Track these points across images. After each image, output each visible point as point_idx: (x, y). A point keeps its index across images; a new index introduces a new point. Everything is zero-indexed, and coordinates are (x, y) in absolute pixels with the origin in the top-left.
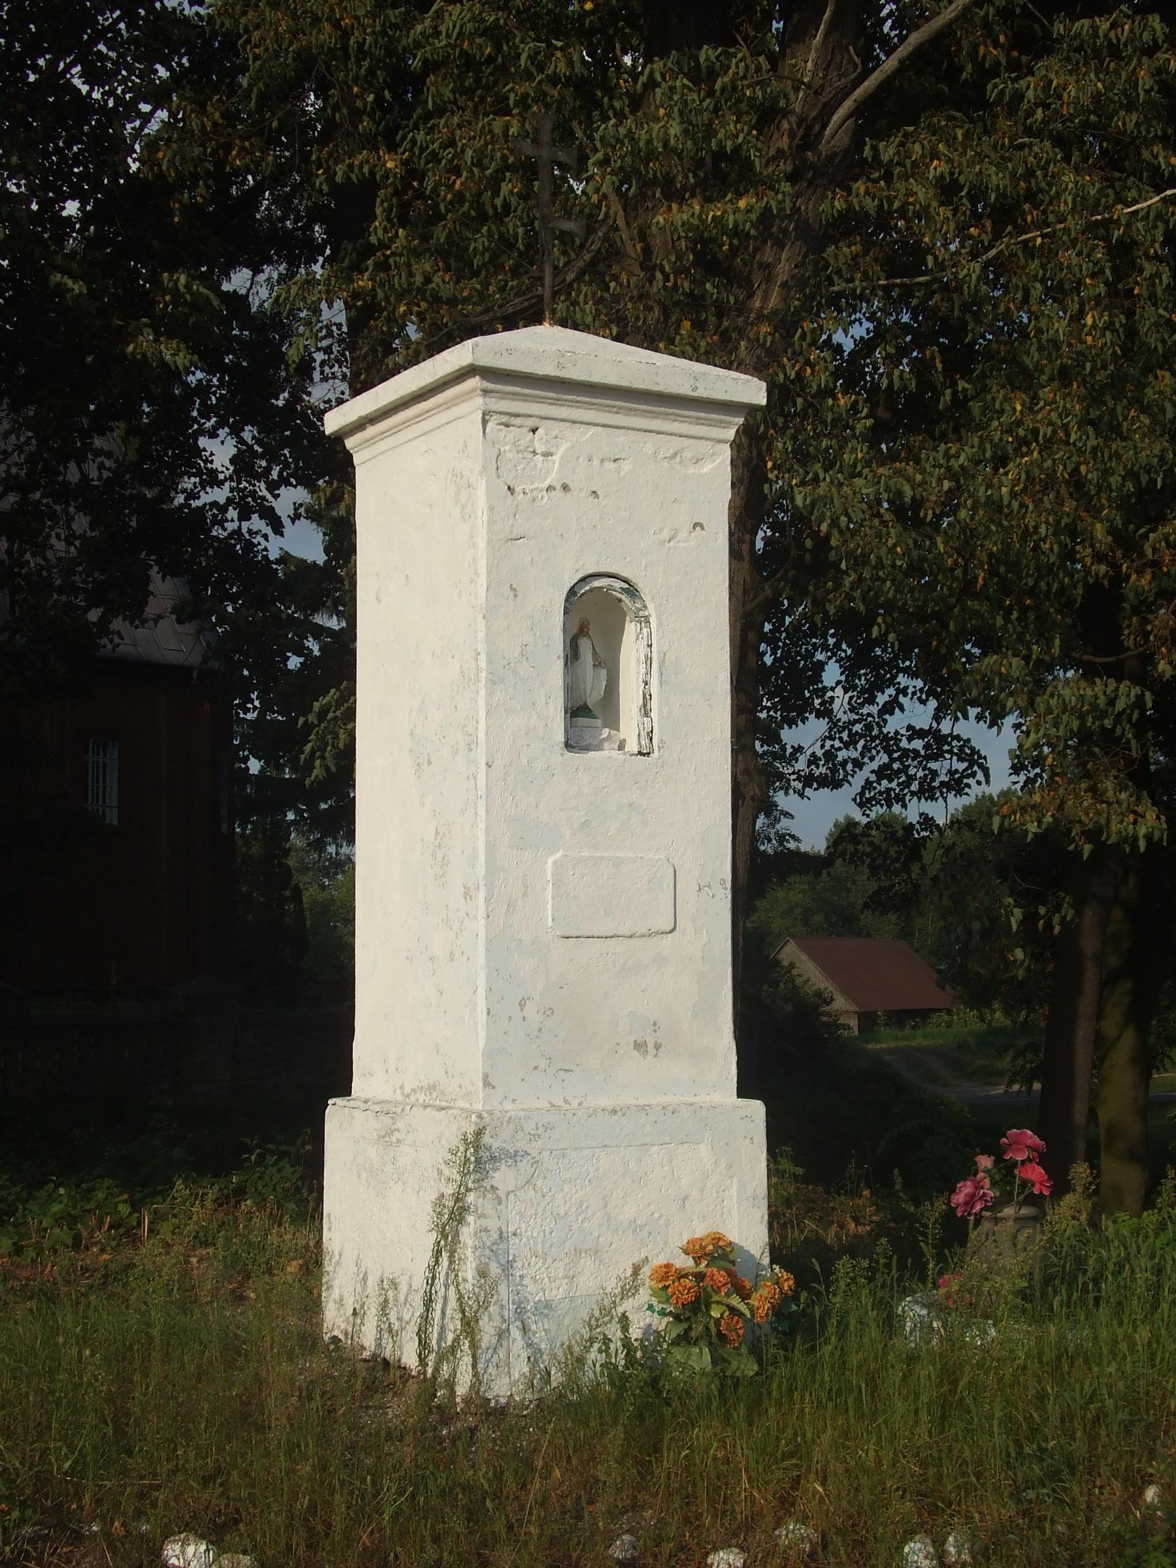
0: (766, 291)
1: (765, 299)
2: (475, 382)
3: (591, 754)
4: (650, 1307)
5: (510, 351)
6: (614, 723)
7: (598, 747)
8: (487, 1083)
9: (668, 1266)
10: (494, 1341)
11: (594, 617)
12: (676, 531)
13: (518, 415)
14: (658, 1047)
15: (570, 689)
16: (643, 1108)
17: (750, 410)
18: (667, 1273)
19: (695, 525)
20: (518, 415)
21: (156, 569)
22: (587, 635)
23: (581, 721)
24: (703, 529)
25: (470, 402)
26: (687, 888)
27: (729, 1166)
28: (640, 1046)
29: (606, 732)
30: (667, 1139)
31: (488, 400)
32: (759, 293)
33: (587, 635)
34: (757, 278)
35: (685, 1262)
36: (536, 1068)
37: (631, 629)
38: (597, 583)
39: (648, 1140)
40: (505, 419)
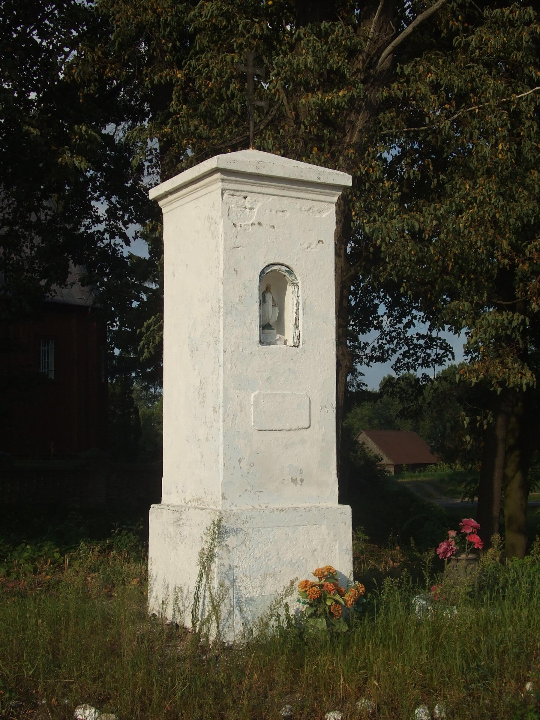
0: (352, 134)
1: (351, 137)
2: (218, 175)
3: (271, 346)
4: (299, 600)
5: (234, 161)
6: (282, 332)
7: (275, 343)
8: (224, 498)
9: (307, 581)
10: (227, 616)
11: (273, 283)
12: (311, 244)
13: (238, 191)
14: (302, 481)
15: (262, 316)
16: (295, 509)
17: (344, 188)
18: (306, 585)
19: (319, 241)
20: (238, 191)
21: (72, 261)
22: (270, 292)
23: (267, 331)
24: (323, 243)
25: (216, 185)
26: (315, 408)
27: (335, 536)
28: (294, 480)
29: (278, 336)
30: (306, 523)
31: (224, 184)
32: (349, 135)
33: (270, 292)
34: (348, 128)
35: (315, 580)
36: (246, 490)
37: (290, 289)
38: (274, 268)
39: (298, 523)
40: (232, 192)
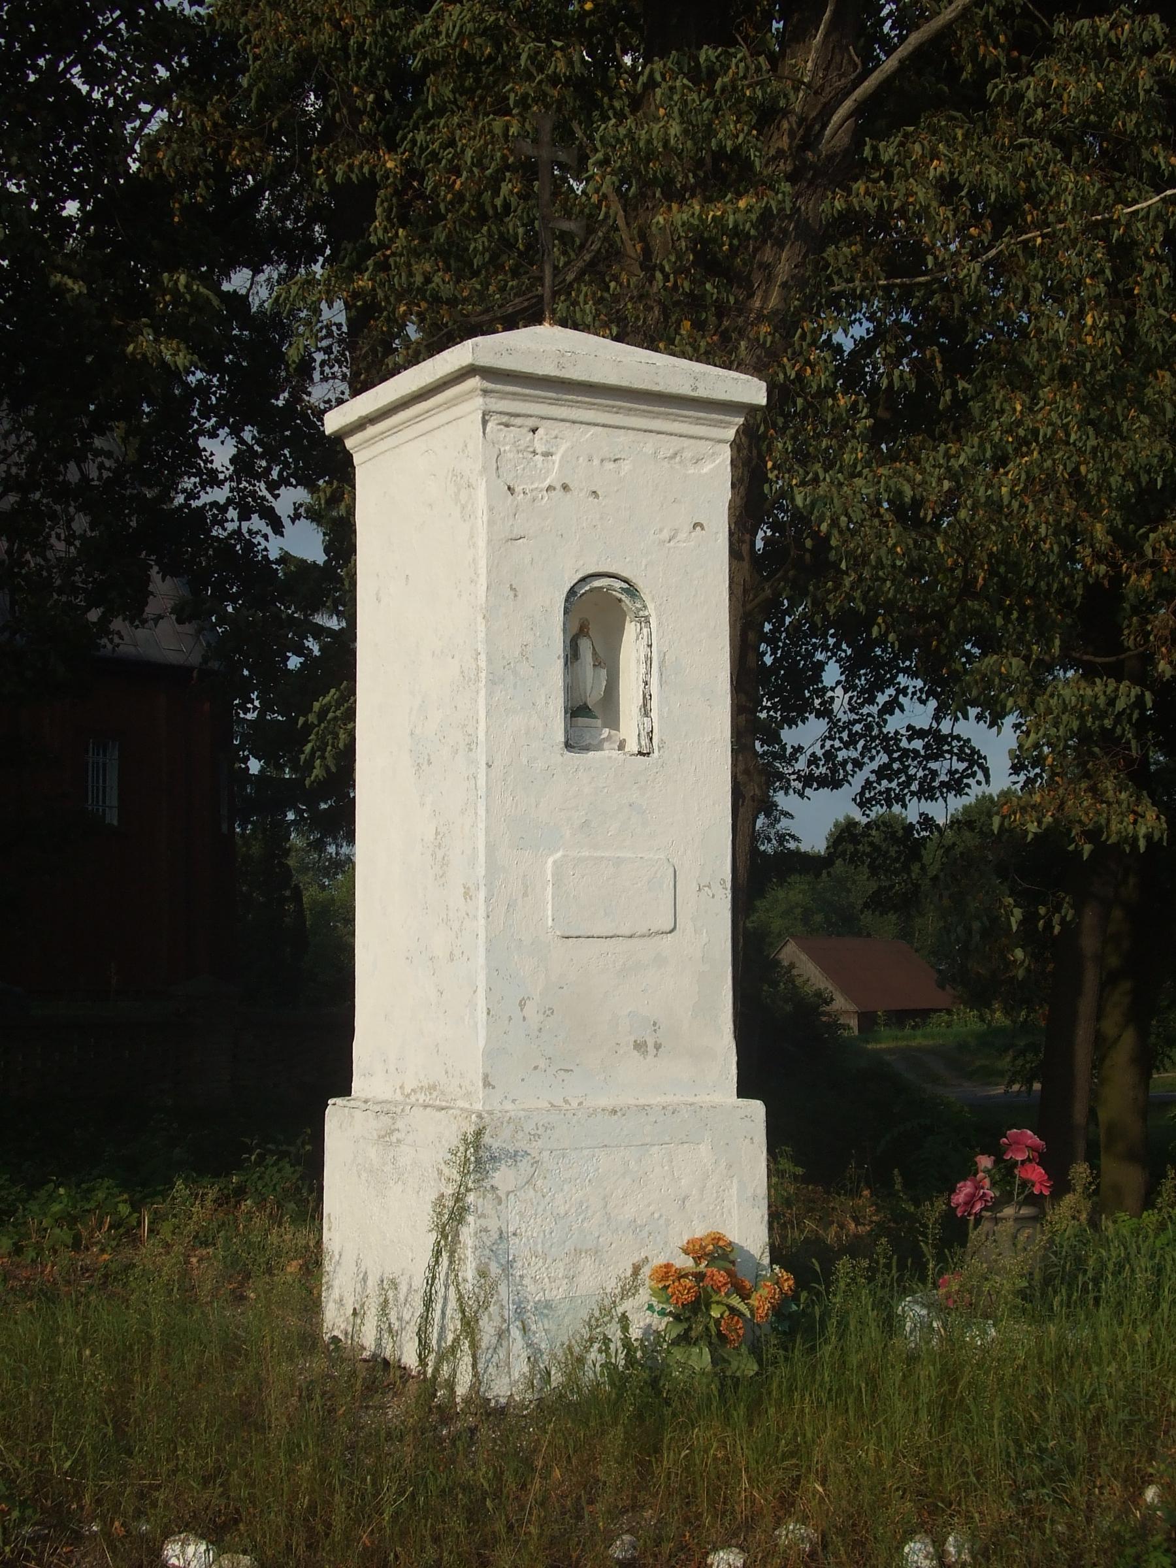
0: (766, 291)
1: (765, 299)
2: (475, 382)
3: (591, 754)
4: (650, 1307)
5: (510, 351)
6: (614, 723)
7: (598, 747)
8: (487, 1083)
9: (668, 1266)
10: (494, 1341)
11: (594, 617)
12: (676, 531)
13: (518, 415)
14: (658, 1047)
15: (570, 689)
16: (643, 1108)
17: (750, 410)
18: (667, 1273)
19: (695, 525)
20: (518, 415)
21: (156, 569)
22: (587, 635)
23: (581, 721)
24: (703, 529)
25: (470, 402)
26: (687, 888)
27: (729, 1166)
28: (640, 1046)
29: (606, 732)
30: (667, 1139)
31: (488, 400)
32: (759, 293)
33: (587, 635)
34: (757, 278)
35: (685, 1262)
36: (536, 1068)
37: (631, 629)
38: (597, 583)
39: (648, 1140)
40: (505, 419)
